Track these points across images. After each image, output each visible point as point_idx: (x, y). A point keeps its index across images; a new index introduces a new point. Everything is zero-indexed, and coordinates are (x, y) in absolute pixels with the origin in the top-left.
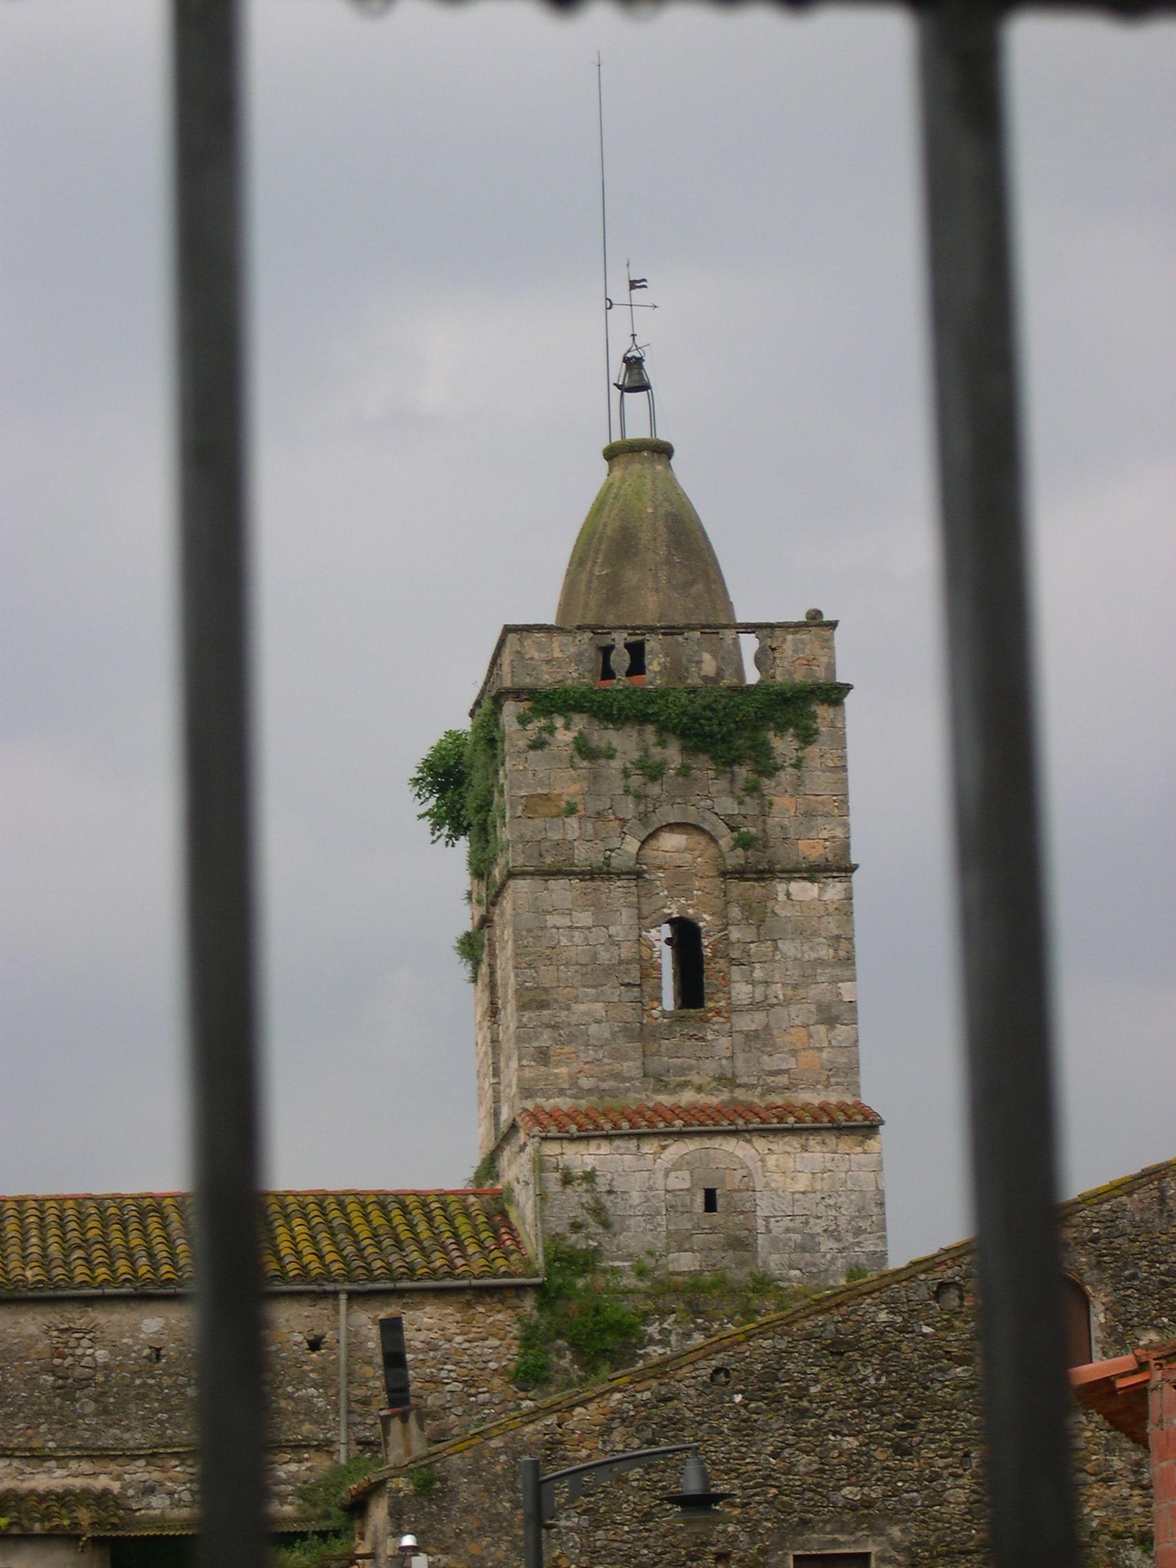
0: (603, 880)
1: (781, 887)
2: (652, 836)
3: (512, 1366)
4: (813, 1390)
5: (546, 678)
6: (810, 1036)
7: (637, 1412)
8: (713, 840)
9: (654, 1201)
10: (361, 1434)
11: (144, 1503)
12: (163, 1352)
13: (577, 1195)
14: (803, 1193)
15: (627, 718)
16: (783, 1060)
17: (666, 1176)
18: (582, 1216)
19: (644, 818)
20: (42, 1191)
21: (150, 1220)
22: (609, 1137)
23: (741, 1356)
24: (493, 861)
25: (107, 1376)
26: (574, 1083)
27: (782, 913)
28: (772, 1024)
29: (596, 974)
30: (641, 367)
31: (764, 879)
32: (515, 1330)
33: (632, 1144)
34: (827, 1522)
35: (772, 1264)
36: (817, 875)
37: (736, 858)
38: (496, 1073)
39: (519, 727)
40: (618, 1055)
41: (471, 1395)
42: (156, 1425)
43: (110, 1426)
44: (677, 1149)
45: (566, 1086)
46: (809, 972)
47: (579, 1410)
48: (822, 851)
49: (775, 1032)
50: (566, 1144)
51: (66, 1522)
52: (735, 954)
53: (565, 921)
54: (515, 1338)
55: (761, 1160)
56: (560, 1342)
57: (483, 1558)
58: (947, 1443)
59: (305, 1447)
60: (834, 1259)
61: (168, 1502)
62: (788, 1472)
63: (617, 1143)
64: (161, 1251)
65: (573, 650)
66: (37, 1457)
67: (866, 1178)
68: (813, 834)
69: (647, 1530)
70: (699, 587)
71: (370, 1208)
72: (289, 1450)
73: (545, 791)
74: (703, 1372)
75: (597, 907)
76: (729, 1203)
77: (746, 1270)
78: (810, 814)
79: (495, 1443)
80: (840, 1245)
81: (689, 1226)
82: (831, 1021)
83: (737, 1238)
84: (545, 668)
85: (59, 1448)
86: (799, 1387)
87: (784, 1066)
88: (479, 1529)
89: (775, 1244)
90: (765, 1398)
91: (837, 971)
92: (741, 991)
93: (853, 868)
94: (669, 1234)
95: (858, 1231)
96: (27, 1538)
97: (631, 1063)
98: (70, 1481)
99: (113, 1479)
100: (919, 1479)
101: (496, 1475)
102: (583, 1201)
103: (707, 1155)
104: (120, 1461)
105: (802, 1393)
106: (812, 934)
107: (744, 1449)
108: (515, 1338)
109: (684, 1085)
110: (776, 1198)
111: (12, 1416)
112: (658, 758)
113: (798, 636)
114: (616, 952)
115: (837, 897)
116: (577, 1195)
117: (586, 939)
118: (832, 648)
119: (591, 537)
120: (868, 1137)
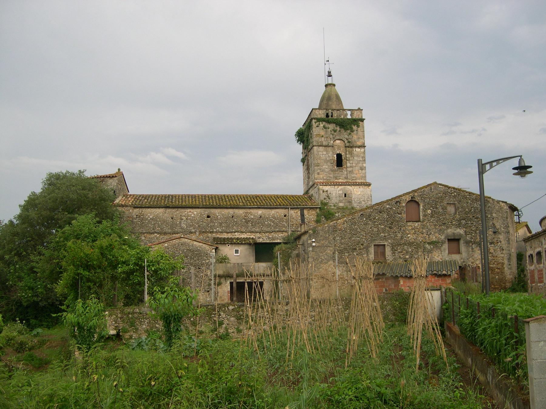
5: (319, 116)
18: (326, 197)
24: (308, 146)
37: (348, 145)
38: (309, 178)
40: (330, 174)
44: (340, 187)
66: (242, 232)
67: (369, 193)
75: (327, 151)
78: (359, 138)
79: (326, 225)
82: (362, 170)
89: (355, 202)
92: (348, 165)
96: (242, 244)
105: (374, 219)
116: (325, 194)
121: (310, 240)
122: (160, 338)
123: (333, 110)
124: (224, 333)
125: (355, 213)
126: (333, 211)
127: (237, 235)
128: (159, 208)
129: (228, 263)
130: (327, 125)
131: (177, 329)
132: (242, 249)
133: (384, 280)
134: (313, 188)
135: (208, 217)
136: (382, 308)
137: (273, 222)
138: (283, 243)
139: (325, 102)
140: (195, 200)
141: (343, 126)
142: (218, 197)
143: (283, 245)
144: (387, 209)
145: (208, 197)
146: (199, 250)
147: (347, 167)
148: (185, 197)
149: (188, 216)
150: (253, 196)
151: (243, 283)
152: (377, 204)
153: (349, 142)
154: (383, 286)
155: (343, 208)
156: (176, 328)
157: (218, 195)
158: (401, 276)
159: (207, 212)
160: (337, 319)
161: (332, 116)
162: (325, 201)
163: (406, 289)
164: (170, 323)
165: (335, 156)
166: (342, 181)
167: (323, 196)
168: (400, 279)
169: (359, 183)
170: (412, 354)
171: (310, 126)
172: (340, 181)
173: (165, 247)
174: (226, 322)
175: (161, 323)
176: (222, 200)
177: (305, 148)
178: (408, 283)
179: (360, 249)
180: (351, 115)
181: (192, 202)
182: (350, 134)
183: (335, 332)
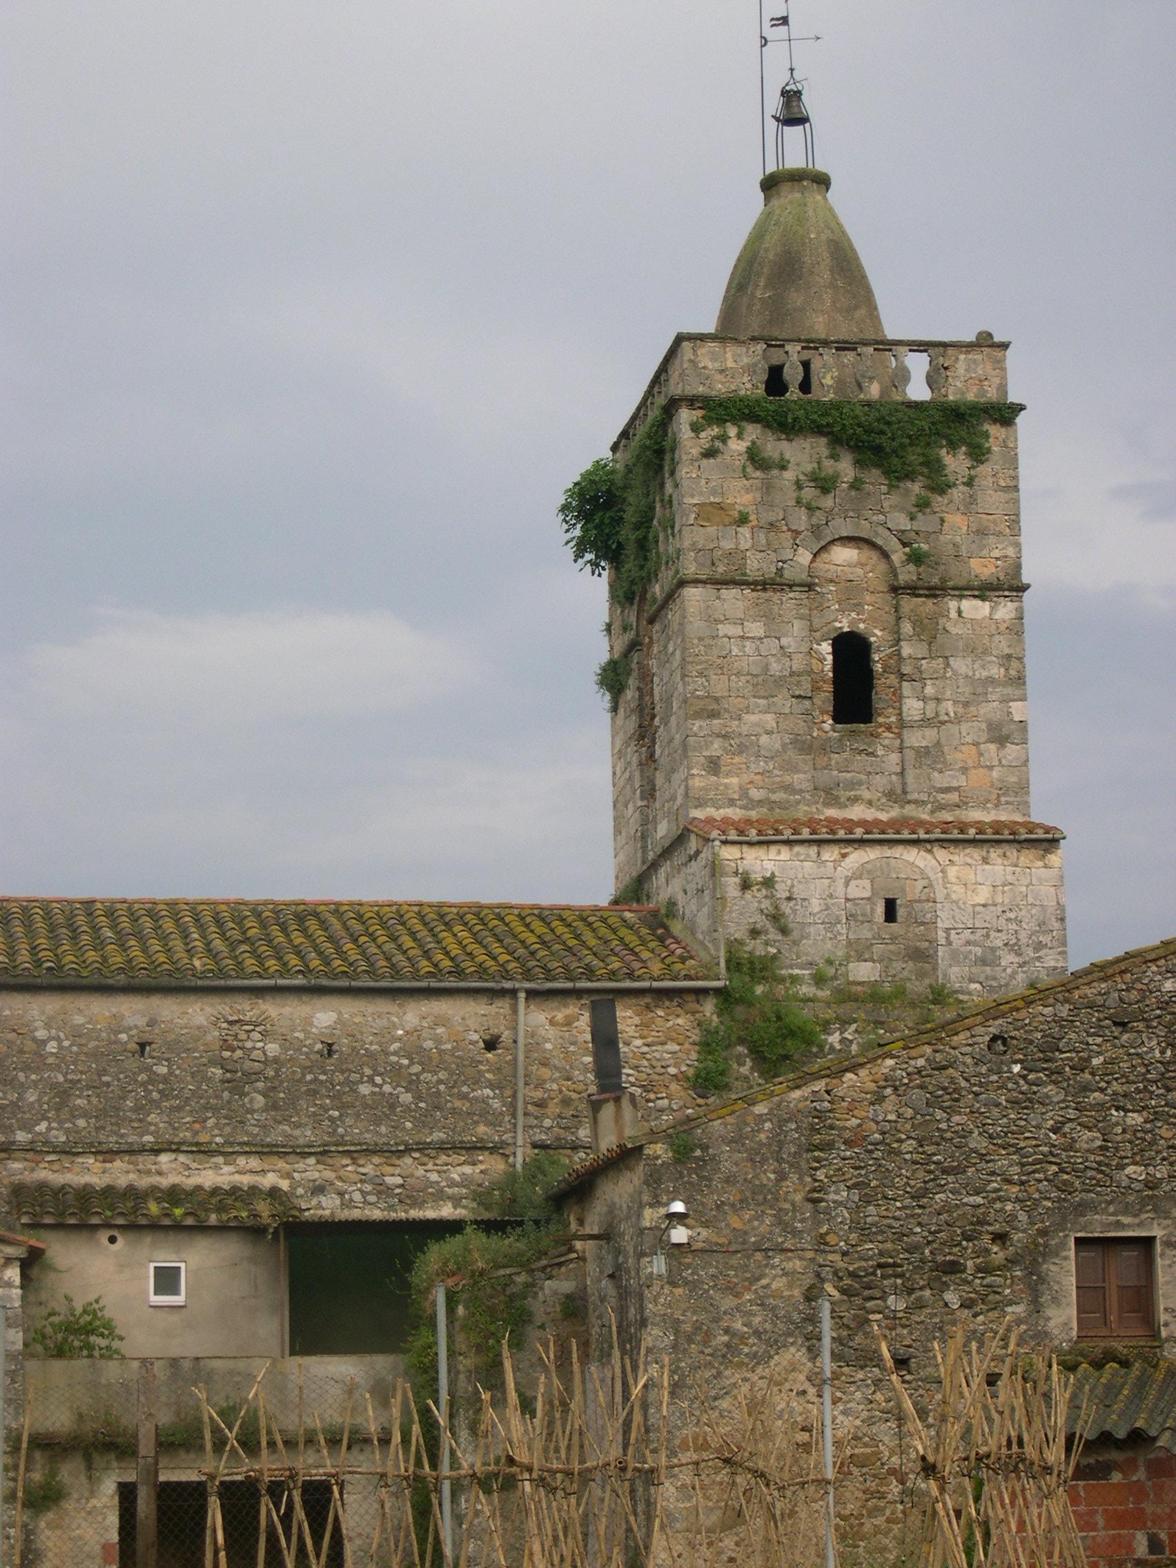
0: (775, 591)
1: (953, 605)
2: (824, 548)
3: (691, 1072)
4: (1095, 1062)
5: (720, 388)
6: (981, 755)
7: (910, 1081)
8: (885, 555)
9: (835, 909)
10: (537, 1138)
11: (314, 1202)
12: (335, 1047)
13: (756, 900)
14: (984, 906)
15: (801, 430)
16: (953, 777)
17: (847, 884)
18: (761, 922)
19: (816, 531)
20: (193, 896)
21: (308, 923)
22: (788, 842)
23: (1019, 1024)
25: (277, 1071)
27: (954, 631)
28: (943, 741)
29: (766, 685)
30: (799, 99)
31: (935, 596)
32: (695, 1036)
33: (813, 850)
35: (952, 977)
36: (988, 593)
37: (907, 574)
39: (693, 435)
40: (792, 768)
41: (648, 1101)
42: (327, 1122)
43: (280, 1123)
45: (736, 797)
46: (980, 690)
47: (849, 1075)
48: (994, 570)
49: (946, 749)
50: (745, 848)
51: (244, 1214)
52: (906, 669)
54: (694, 1044)
55: (942, 871)
57: (746, 1233)
59: (481, 1148)
60: (1015, 973)
61: (338, 1202)
62: (1070, 1147)
63: (797, 849)
64: (329, 949)
65: (746, 360)
66: (203, 1151)
68: (985, 553)
69: (920, 1207)
70: (862, 312)
71: (528, 920)
72: (464, 1152)
73: (717, 500)
74: (980, 1039)
75: (768, 618)
76: (909, 914)
78: (982, 532)
79: (761, 1109)
80: (1021, 960)
81: (869, 935)
83: (917, 949)
84: (719, 377)
85: (227, 1143)
86: (1081, 1058)
87: (955, 784)
88: (741, 1201)
89: (955, 956)
90: (1045, 1069)
91: (1008, 690)
92: (912, 707)
93: (1024, 588)
94: (849, 944)
95: (1039, 946)
96: (202, 1229)
97: (801, 776)
98: (237, 1177)
99: (282, 1177)
101: (761, 1144)
102: (763, 906)
103: (888, 864)
106: (983, 653)
107: (1023, 1123)
108: (694, 1044)
109: (855, 800)
110: (957, 911)
111: (179, 1109)
112: (830, 471)
113: (970, 356)
114: (788, 664)
115: (1007, 617)
116: (756, 900)
117: (758, 649)
118: (1004, 369)
147: (902, 724)
180: (931, 381)
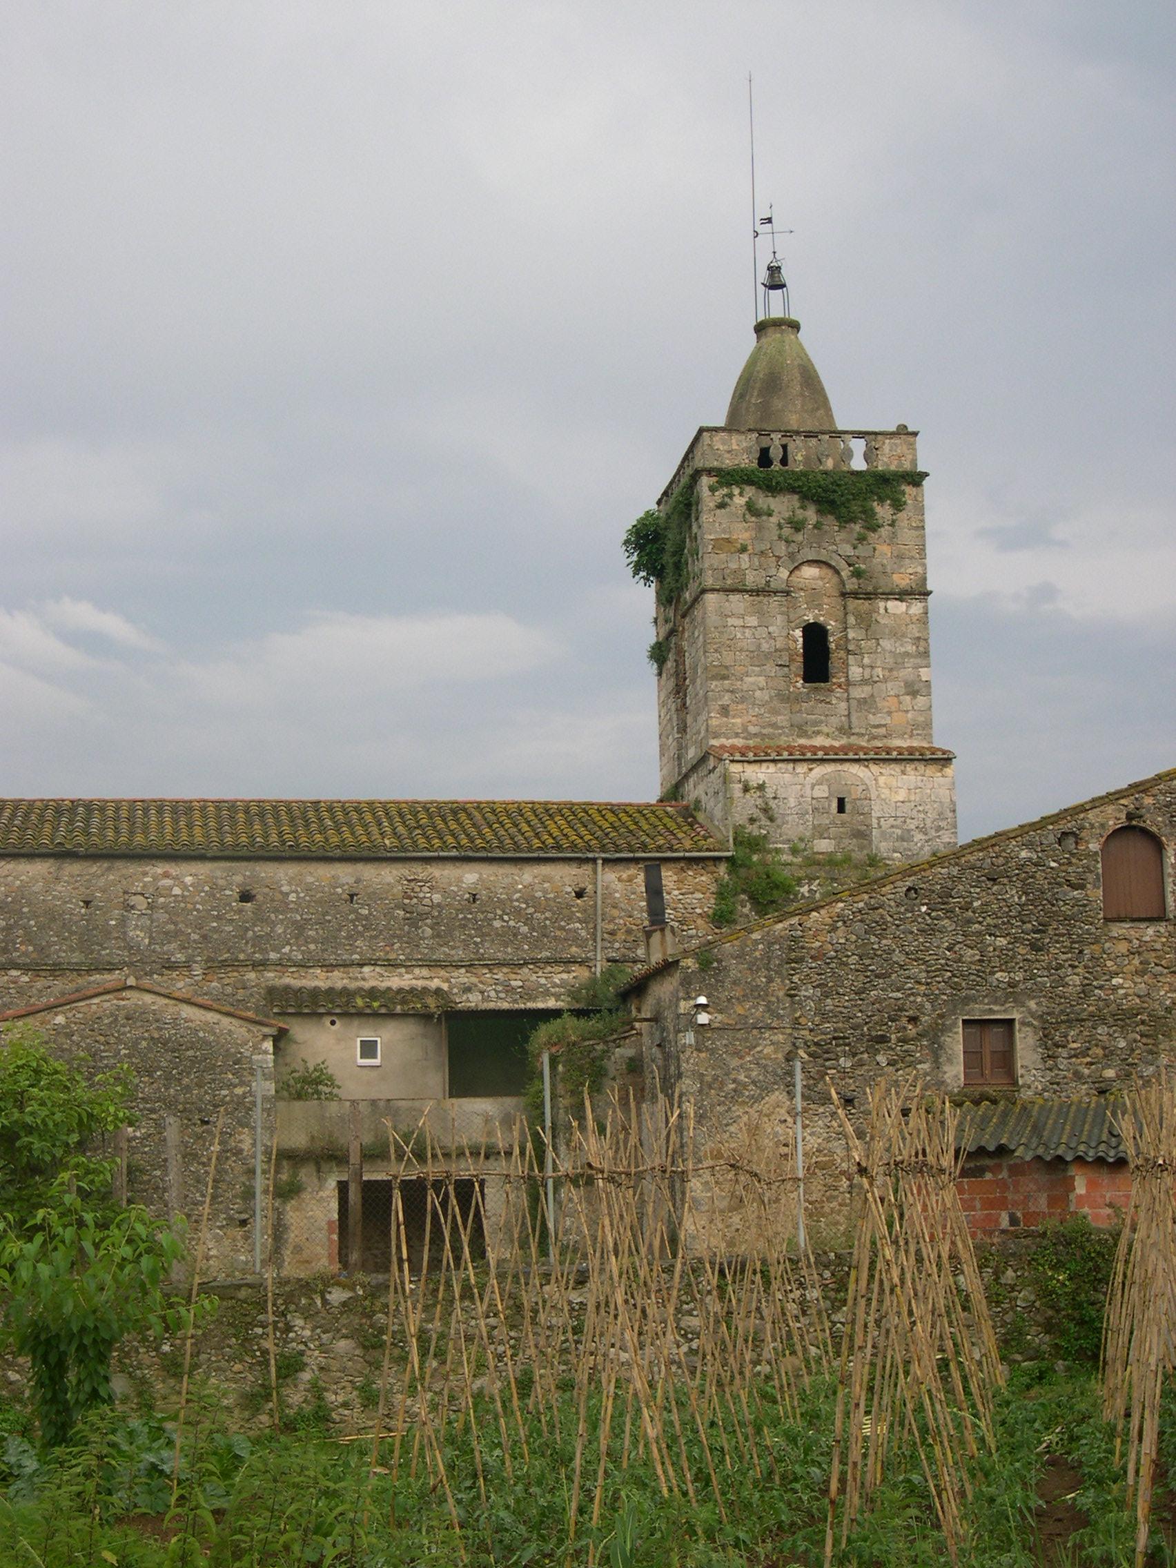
1: (882, 604)
3: (711, 912)
4: (976, 904)
5: (728, 463)
8: (837, 572)
15: (781, 490)
18: (757, 813)
24: (682, 589)
26: (745, 729)
27: (882, 622)
33: (791, 766)
34: (985, 997)
38: (683, 729)
40: (775, 712)
44: (819, 771)
47: (814, 914)
53: (740, 622)
56: (743, 896)
58: (1067, 944)
63: (780, 765)
66: (392, 965)
67: (944, 794)
70: (822, 411)
75: (761, 613)
77: (865, 852)
78: (901, 557)
82: (914, 693)
84: (727, 455)
87: (883, 722)
91: (918, 661)
92: (855, 672)
94: (814, 827)
95: (939, 829)
96: (391, 1015)
98: (414, 982)
100: (1048, 969)
104: (449, 969)
109: (818, 733)
111: (376, 937)
116: (753, 798)
118: (915, 450)
119: (748, 380)
120: (944, 766)
121: (689, 998)
122: (25, 1432)
123: (788, 433)
124: (308, 1409)
125: (881, 882)
126: (786, 873)
127: (371, 978)
128: (31, 856)
129: (331, 1097)
130: (763, 501)
131: (95, 1394)
132: (391, 1037)
133: (1004, 1174)
134: (702, 771)
135: (246, 897)
136: (993, 1299)
137: (528, 921)
138: (569, 1010)
139: (755, 400)
140: (190, 826)
141: (832, 502)
142: (289, 811)
143: (569, 1021)
144: (1021, 867)
145: (247, 812)
146: (206, 1042)
147: (849, 683)
148: (146, 811)
149: (158, 892)
150: (440, 806)
151: (386, 1186)
152: (979, 845)
153: (857, 574)
154: (1002, 1204)
155: (830, 862)
156: (87, 1387)
157: (288, 804)
158: (1080, 1160)
159: (240, 874)
160: (798, 1348)
161: (784, 461)
162: (754, 830)
163: (1097, 1217)
164: (61, 1367)
165: (798, 633)
166: (827, 742)
167: (744, 807)
168: (1073, 1171)
169: (900, 750)
170: (1121, 1504)
171: (688, 505)
172: (819, 741)
173: (57, 1029)
174: (314, 1358)
175: (25, 1360)
176: (307, 824)
177: (667, 599)
178: (1111, 1188)
179: (904, 1041)
181: (176, 831)
182: (862, 539)
183: (787, 1405)
